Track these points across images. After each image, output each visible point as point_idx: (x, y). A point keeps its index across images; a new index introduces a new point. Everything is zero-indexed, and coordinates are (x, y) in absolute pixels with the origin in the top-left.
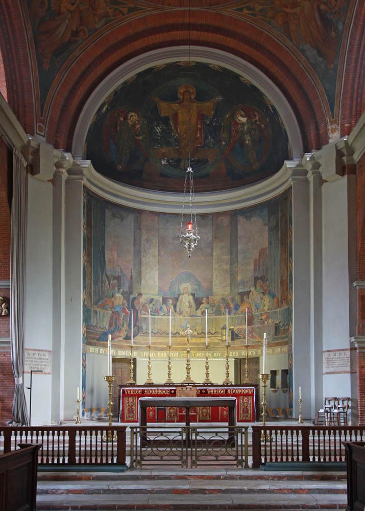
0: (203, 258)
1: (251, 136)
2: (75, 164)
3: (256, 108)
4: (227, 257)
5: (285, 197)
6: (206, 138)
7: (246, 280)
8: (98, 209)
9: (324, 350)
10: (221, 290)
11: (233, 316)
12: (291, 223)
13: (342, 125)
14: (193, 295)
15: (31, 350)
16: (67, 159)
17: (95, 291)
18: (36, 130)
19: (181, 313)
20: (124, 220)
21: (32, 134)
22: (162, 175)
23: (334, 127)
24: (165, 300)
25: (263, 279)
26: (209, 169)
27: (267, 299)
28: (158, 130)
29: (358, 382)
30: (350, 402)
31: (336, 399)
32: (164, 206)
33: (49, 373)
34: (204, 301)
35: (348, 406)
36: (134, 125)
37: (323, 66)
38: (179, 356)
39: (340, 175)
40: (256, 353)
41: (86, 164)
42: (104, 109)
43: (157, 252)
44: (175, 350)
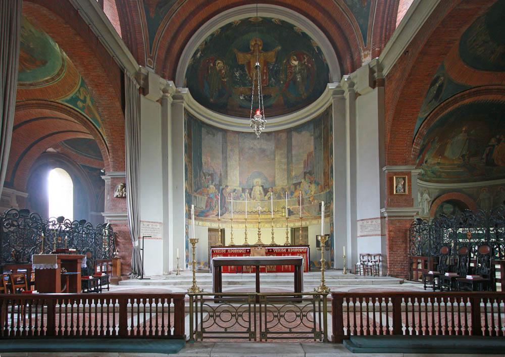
0: (269, 162)
1: (301, 75)
2: (178, 92)
3: (305, 52)
4: (284, 160)
5: (327, 114)
6: (270, 79)
7: (298, 175)
8: (194, 126)
9: (358, 219)
10: (281, 182)
11: (289, 199)
12: (331, 130)
13: (373, 50)
14: (262, 186)
15: (146, 222)
16: (171, 85)
17: (195, 183)
18: (147, 60)
19: (254, 199)
20: (216, 136)
21: (144, 66)
22: (240, 107)
23: (366, 53)
24: (243, 190)
25: (310, 173)
26: (272, 102)
27: (313, 186)
28: (237, 74)
29: (387, 242)
30: (381, 257)
31: (369, 255)
32: (243, 127)
33: (160, 239)
34: (270, 190)
35: (380, 260)
36: (220, 70)
37: (358, 6)
38: (254, 226)
39: (372, 87)
40: (306, 224)
41: (185, 91)
42: (199, 55)
43: (238, 158)
44: (251, 223)
